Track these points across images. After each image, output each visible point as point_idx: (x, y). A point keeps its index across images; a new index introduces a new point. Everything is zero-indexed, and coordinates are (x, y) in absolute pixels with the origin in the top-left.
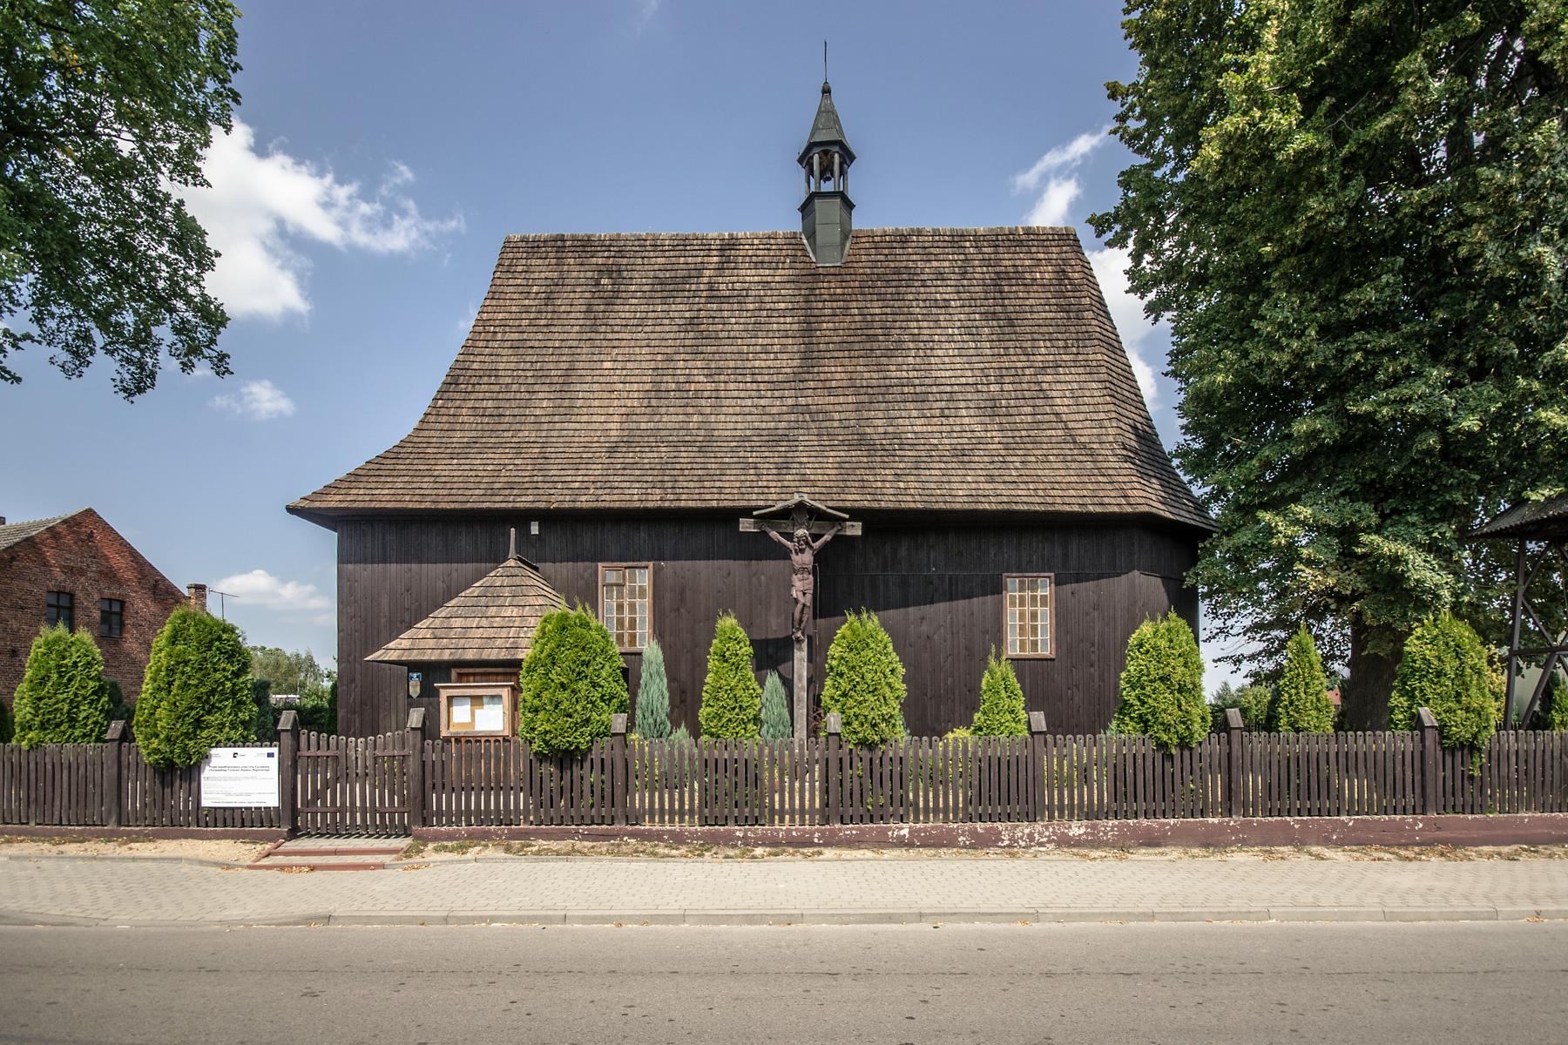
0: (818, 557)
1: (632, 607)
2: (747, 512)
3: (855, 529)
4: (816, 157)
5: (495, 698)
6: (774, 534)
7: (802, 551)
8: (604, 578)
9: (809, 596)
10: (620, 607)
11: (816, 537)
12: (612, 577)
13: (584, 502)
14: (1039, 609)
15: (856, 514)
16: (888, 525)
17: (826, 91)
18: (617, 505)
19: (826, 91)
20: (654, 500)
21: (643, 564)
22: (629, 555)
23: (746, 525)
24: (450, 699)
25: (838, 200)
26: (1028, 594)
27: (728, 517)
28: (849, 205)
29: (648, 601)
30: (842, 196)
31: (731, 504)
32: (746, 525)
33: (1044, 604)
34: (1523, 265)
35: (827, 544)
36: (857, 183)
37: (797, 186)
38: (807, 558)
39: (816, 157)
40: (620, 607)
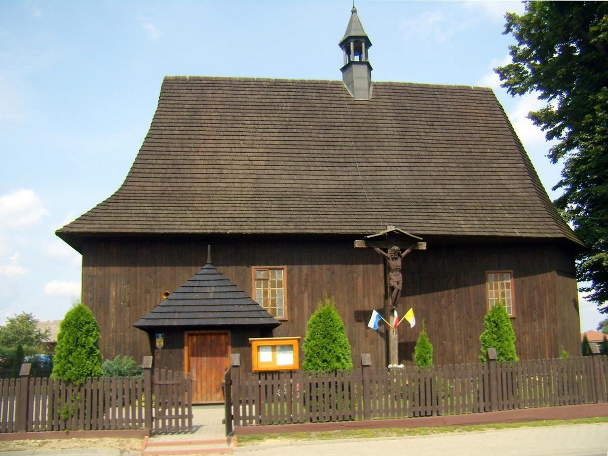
0: (404, 260)
1: (273, 293)
2: (361, 237)
3: (423, 246)
4: (352, 44)
5: (290, 347)
6: (378, 249)
7: (396, 259)
8: (255, 276)
9: (400, 285)
10: (266, 293)
11: (403, 251)
12: (261, 275)
13: (246, 230)
14: (505, 290)
15: (426, 238)
16: (443, 245)
17: (354, 11)
18: (140, 231)
19: (354, 11)
20: (291, 229)
21: (281, 267)
22: (272, 261)
23: (358, 244)
24: (259, 347)
25: (366, 66)
26: (499, 283)
27: (347, 240)
28: (370, 69)
29: (284, 289)
30: (368, 64)
31: (329, 231)
32: (358, 244)
33: (508, 288)
34: (505, 78)
35: (408, 254)
36: (373, 55)
37: (340, 58)
38: (398, 263)
39: (352, 44)
40: (266, 293)
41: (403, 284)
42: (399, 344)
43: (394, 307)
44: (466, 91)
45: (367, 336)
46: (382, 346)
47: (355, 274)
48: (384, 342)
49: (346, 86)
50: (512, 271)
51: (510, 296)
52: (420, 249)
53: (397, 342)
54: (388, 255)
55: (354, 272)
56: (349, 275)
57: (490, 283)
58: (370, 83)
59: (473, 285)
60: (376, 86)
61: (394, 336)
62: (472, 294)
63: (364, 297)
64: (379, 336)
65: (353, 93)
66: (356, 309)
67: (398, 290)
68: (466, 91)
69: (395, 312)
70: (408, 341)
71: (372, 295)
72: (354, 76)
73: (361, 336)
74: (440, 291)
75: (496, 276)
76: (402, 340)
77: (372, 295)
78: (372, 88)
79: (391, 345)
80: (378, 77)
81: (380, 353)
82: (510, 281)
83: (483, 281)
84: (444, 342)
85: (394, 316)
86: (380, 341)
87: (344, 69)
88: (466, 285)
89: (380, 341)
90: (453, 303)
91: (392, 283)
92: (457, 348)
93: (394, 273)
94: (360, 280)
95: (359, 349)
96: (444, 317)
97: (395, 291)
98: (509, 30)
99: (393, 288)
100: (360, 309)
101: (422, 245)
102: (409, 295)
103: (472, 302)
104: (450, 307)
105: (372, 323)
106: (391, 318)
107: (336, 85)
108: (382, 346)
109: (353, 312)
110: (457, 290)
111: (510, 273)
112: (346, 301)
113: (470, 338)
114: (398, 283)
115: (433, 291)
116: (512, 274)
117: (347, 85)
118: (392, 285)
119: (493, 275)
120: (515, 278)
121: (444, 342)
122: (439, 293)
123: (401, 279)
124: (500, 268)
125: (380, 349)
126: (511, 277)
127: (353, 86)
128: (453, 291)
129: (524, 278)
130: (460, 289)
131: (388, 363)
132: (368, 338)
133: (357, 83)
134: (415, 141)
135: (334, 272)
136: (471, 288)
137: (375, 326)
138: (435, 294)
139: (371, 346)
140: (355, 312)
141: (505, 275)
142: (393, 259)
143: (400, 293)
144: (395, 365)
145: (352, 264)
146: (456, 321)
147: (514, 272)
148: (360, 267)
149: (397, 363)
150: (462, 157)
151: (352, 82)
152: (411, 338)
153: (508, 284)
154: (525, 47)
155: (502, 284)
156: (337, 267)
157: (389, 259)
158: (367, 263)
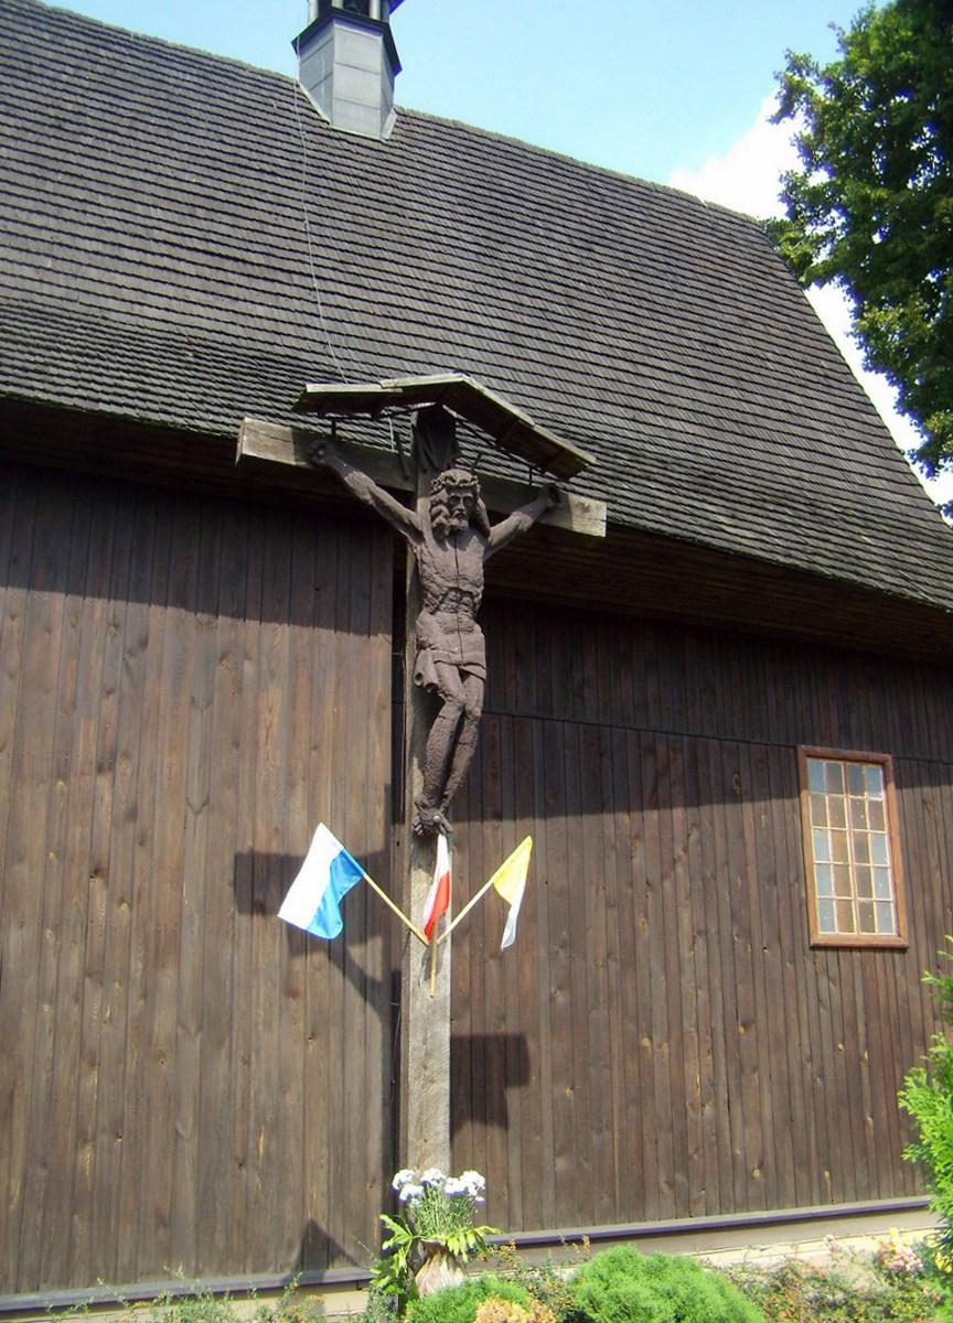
0: (496, 564)
25: (379, 39)
26: (847, 800)
35: (517, 537)
38: (469, 561)
41: (490, 684)
42: (455, 1042)
43: (437, 816)
44: (685, 203)
45: (291, 992)
46: (366, 1044)
47: (248, 667)
48: (377, 1029)
49: (306, 92)
50: (889, 757)
51: (884, 857)
52: (577, 528)
53: (444, 1031)
54: (420, 514)
55: (247, 656)
56: (221, 670)
57: (814, 797)
58: (387, 105)
59: (752, 800)
60: (405, 118)
61: (430, 994)
62: (749, 835)
63: (291, 785)
64: (355, 997)
65: (329, 107)
66: (245, 846)
67: (464, 715)
68: (685, 203)
69: (442, 841)
70: (491, 1030)
71: (326, 777)
72: (337, 57)
73: (265, 992)
74: (629, 811)
75: (834, 775)
76: (465, 1030)
77: (326, 777)
78: (392, 118)
79: (414, 1044)
80: (412, 94)
81: (355, 1100)
82: (881, 797)
83: (790, 785)
84: (646, 1042)
85: (430, 866)
86: (358, 1021)
87: (304, 42)
88: (732, 796)
89: (358, 1021)
90: (680, 869)
91: (429, 670)
92: (695, 1075)
93: (445, 616)
94: (275, 696)
95: (247, 1062)
96: (646, 930)
97: (449, 714)
98: (787, 110)
99: (432, 699)
100: (261, 848)
101: (586, 509)
102: (499, 816)
103: (752, 870)
104: (667, 884)
105: (311, 900)
106: (418, 879)
107: (277, 83)
108: (366, 1044)
109: (229, 859)
110: (692, 811)
111: (882, 764)
112: (196, 800)
113: (745, 1026)
114: (464, 675)
115: (600, 807)
116: (890, 764)
117: (310, 90)
118: (431, 677)
119: (824, 763)
120: (899, 786)
121: (646, 1042)
122: (624, 818)
123: (481, 655)
124: (850, 741)
125: (356, 1061)
126: (886, 783)
127: (330, 89)
128: (678, 813)
129: (927, 790)
130: (705, 809)
131: (393, 1159)
132: (294, 1004)
133: (343, 81)
134: (533, 272)
135: (144, 643)
136: (747, 807)
137: (321, 919)
138: (608, 818)
139: (313, 1046)
140: (238, 858)
141: (866, 769)
142: (438, 532)
143: (470, 733)
144: (432, 1174)
145: (241, 614)
146: (692, 948)
147: (896, 759)
148: (281, 637)
149: (446, 1163)
150: (690, 352)
151: (329, 75)
152: (503, 1018)
153: (876, 806)
154: (820, 178)
155: (858, 808)
156: (160, 619)
157: (419, 536)
158: (315, 621)
